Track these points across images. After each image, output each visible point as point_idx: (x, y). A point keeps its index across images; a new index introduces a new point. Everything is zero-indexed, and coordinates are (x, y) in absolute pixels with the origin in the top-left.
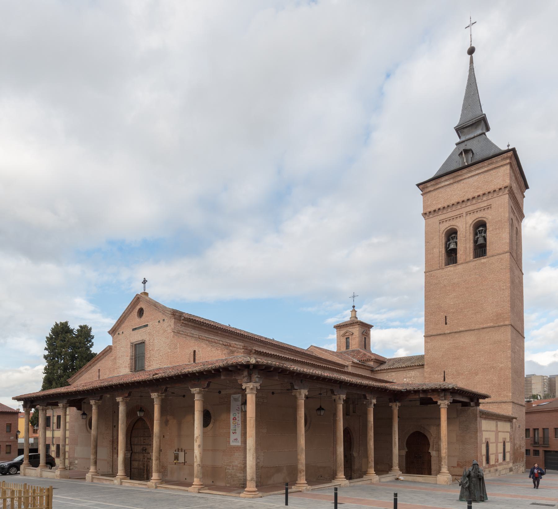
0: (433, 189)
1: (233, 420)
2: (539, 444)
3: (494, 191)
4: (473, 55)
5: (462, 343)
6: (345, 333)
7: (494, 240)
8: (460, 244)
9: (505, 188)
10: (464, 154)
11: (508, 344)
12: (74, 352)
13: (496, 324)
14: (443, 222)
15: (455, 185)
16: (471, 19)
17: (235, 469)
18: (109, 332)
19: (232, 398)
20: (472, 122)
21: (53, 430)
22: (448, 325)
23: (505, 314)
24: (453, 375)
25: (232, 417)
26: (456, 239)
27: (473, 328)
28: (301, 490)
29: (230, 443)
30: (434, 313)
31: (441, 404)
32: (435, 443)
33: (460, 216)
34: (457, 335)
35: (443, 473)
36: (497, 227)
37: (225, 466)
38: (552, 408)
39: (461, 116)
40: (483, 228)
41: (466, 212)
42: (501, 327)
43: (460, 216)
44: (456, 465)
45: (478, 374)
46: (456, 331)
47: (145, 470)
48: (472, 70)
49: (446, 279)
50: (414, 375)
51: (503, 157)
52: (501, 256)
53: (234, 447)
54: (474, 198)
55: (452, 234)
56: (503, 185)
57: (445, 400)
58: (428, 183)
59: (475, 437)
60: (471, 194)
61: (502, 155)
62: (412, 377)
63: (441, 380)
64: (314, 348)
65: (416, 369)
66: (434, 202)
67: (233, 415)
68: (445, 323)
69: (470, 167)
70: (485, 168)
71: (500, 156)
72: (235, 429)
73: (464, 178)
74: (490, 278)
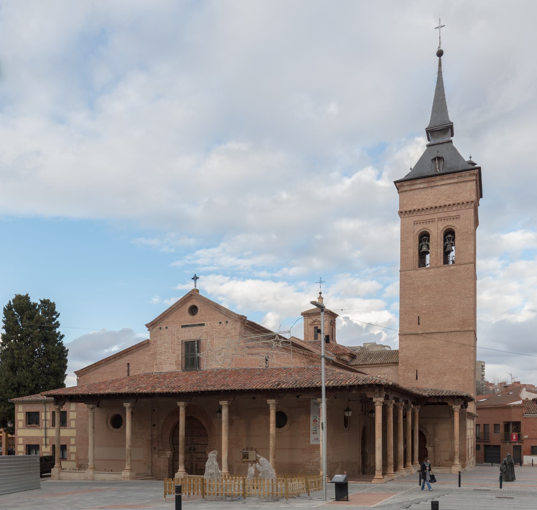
0: (409, 189)
1: (313, 422)
2: (480, 439)
3: (463, 203)
4: (441, 58)
5: (433, 344)
6: (314, 322)
7: (462, 250)
8: (432, 248)
9: (472, 203)
10: (438, 161)
11: (472, 349)
12: (44, 333)
13: (462, 328)
14: (417, 223)
15: (428, 190)
16: (440, 20)
17: (315, 465)
18: (147, 326)
19: (312, 403)
20: (442, 127)
21: (46, 429)
22: (420, 326)
23: (469, 321)
24: (424, 374)
25: (312, 419)
26: (428, 242)
27: (443, 331)
28: (393, 478)
29: (310, 442)
30: (408, 312)
31: (455, 408)
32: (431, 440)
33: (433, 221)
34: (429, 336)
35: (456, 465)
36: (464, 238)
37: (305, 462)
38: (492, 405)
39: (431, 118)
40: (451, 235)
41: (438, 218)
42: (466, 332)
43: (433, 221)
44: (449, 459)
45: (446, 374)
46: (428, 332)
47: (194, 470)
48: (440, 73)
49: (420, 280)
50: (387, 372)
51: (470, 173)
52: (467, 266)
53: (314, 446)
54: (445, 206)
55: (424, 237)
56: (469, 199)
57: (458, 405)
58: (405, 182)
59: (464, 434)
60: (443, 201)
61: (470, 171)
62: (386, 374)
63: (414, 379)
64: (295, 339)
65: (390, 366)
66: (410, 203)
67: (313, 417)
68: (418, 323)
69: (443, 176)
70: (455, 179)
71: (468, 172)
72: (316, 430)
73: (437, 185)
74: (458, 285)
